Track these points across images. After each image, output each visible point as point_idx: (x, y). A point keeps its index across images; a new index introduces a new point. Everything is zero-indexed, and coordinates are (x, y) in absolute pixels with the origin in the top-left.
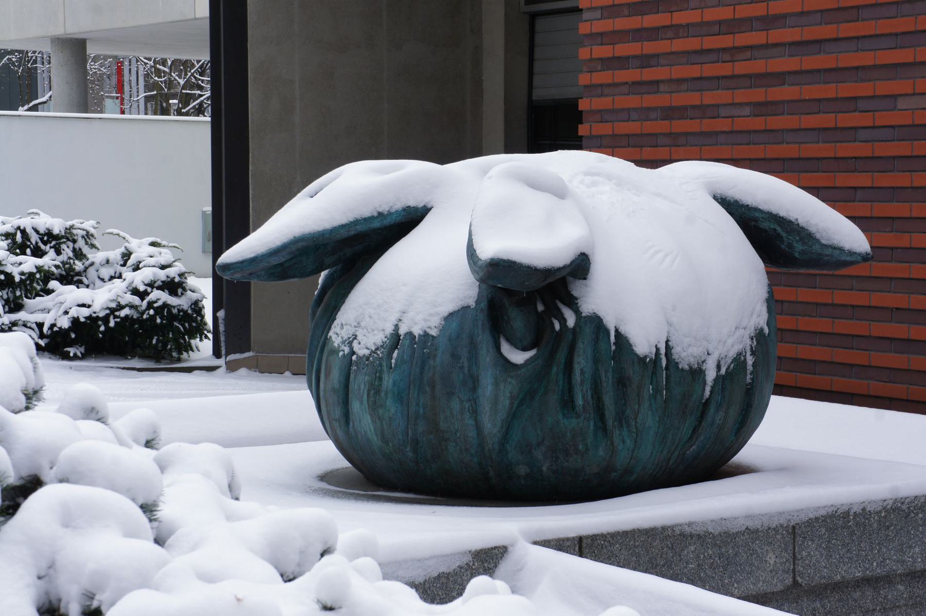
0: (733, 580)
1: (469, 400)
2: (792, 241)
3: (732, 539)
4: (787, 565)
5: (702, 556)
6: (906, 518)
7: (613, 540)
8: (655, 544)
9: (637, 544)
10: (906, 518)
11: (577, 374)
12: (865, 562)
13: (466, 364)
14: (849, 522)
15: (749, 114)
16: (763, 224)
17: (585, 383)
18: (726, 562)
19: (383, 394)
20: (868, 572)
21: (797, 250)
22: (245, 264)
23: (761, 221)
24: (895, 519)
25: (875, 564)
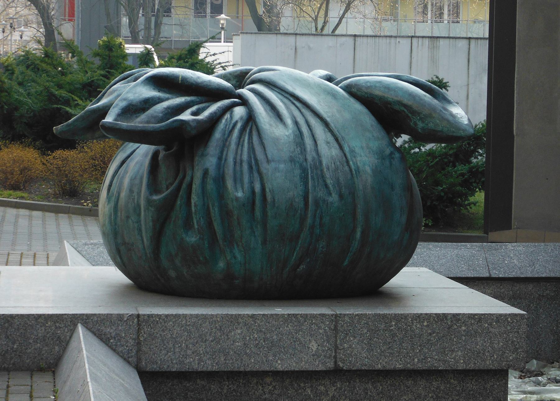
0: (277, 358)
1: (138, 222)
3: (277, 328)
5: (248, 338)
6: (449, 328)
7: (167, 318)
9: (188, 323)
13: (136, 197)
18: (270, 345)
24: (437, 328)
25: (416, 360)
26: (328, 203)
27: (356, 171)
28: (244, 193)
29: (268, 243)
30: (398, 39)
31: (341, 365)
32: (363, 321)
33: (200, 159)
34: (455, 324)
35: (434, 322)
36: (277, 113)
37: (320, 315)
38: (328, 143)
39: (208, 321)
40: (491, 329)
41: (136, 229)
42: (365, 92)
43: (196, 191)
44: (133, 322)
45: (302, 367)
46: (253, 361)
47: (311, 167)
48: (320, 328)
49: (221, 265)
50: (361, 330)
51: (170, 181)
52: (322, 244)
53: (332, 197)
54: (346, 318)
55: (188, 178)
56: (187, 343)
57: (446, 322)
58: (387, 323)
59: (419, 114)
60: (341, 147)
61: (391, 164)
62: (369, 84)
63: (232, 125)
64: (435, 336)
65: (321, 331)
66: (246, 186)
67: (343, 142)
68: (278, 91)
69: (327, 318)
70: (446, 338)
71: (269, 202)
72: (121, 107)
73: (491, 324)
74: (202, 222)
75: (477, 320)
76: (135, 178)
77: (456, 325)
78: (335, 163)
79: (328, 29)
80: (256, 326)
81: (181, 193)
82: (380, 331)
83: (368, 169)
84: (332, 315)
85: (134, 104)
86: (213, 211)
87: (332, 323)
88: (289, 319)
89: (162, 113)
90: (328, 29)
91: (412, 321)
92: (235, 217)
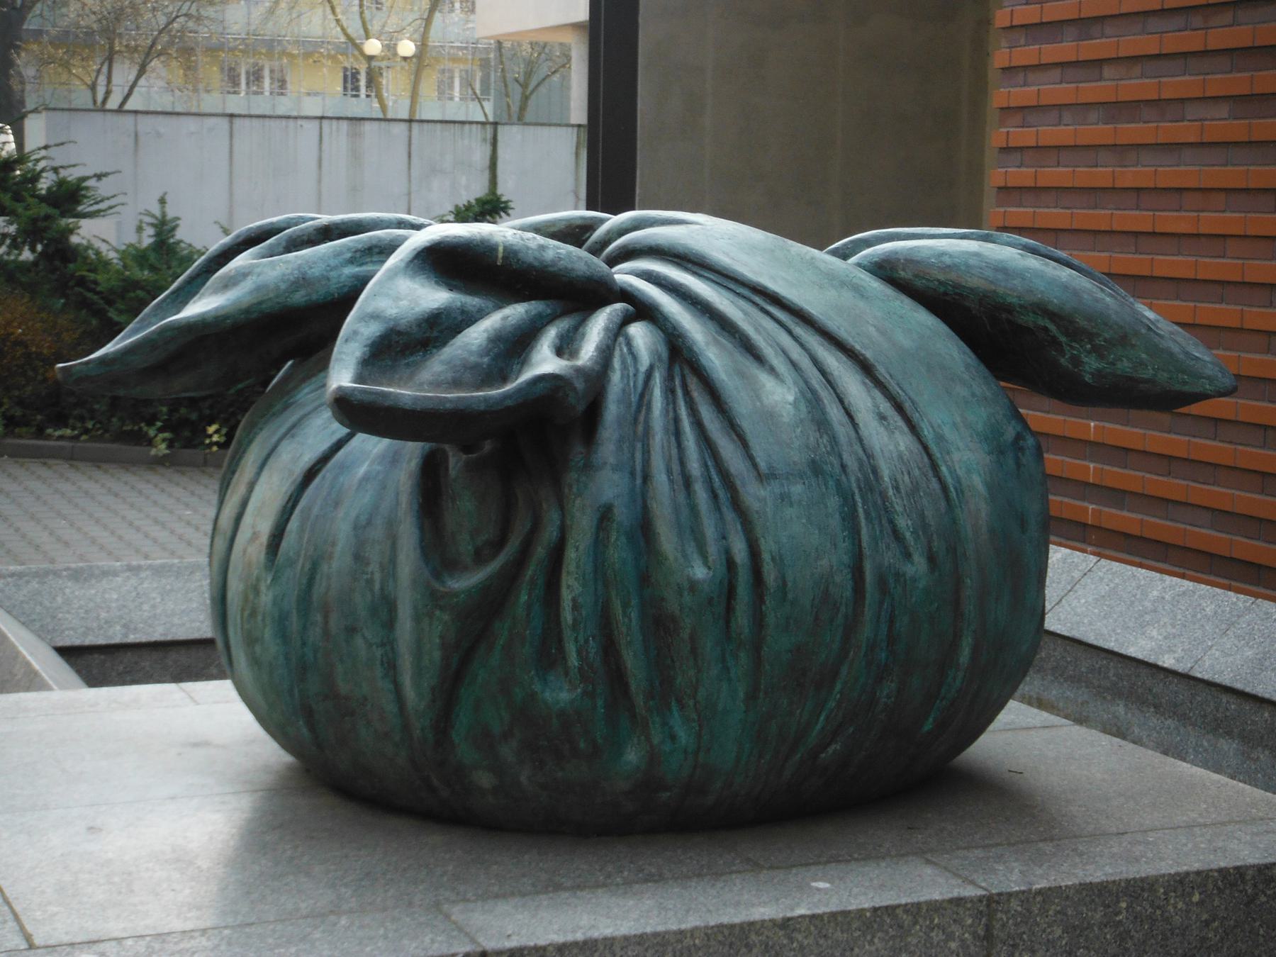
1: (383, 645)
2: (1079, 351)
3: (845, 950)
10: (1247, 904)
11: (567, 608)
13: (377, 576)
14: (1117, 914)
15: (1227, 116)
16: (1022, 317)
17: (582, 625)
19: (260, 618)
21: (1087, 368)
22: (91, 366)
23: (1018, 312)
24: (1223, 907)
26: (905, 581)
27: (956, 489)
28: (709, 568)
29: (761, 694)
30: (300, 122)
32: (1053, 907)
33: (584, 478)
34: (1264, 892)
35: (1215, 892)
36: (741, 340)
37: (951, 901)
38: (882, 418)
39: (670, 948)
41: (378, 662)
42: (938, 280)
43: (578, 567)
47: (860, 489)
48: (950, 937)
49: (632, 756)
50: (1049, 930)
51: (487, 536)
52: (888, 689)
53: (912, 564)
54: (1015, 905)
55: (550, 533)
57: (1241, 888)
58: (1109, 907)
59: (1091, 336)
60: (913, 428)
61: (1018, 464)
62: (947, 260)
63: (641, 378)
64: (1217, 928)
66: (713, 549)
67: (917, 414)
68: (718, 281)
69: (969, 909)
70: (1242, 931)
71: (772, 591)
72: (368, 339)
74: (593, 651)
76: (369, 523)
77: (1265, 895)
78: (909, 474)
79: (113, 103)
80: (794, 950)
81: (530, 573)
82: (1093, 930)
83: (977, 482)
84: (980, 899)
85: (402, 328)
86: (626, 620)
87: (980, 921)
88: (875, 921)
89: (488, 355)
90: (113, 103)
91: (1165, 893)
92: (685, 634)
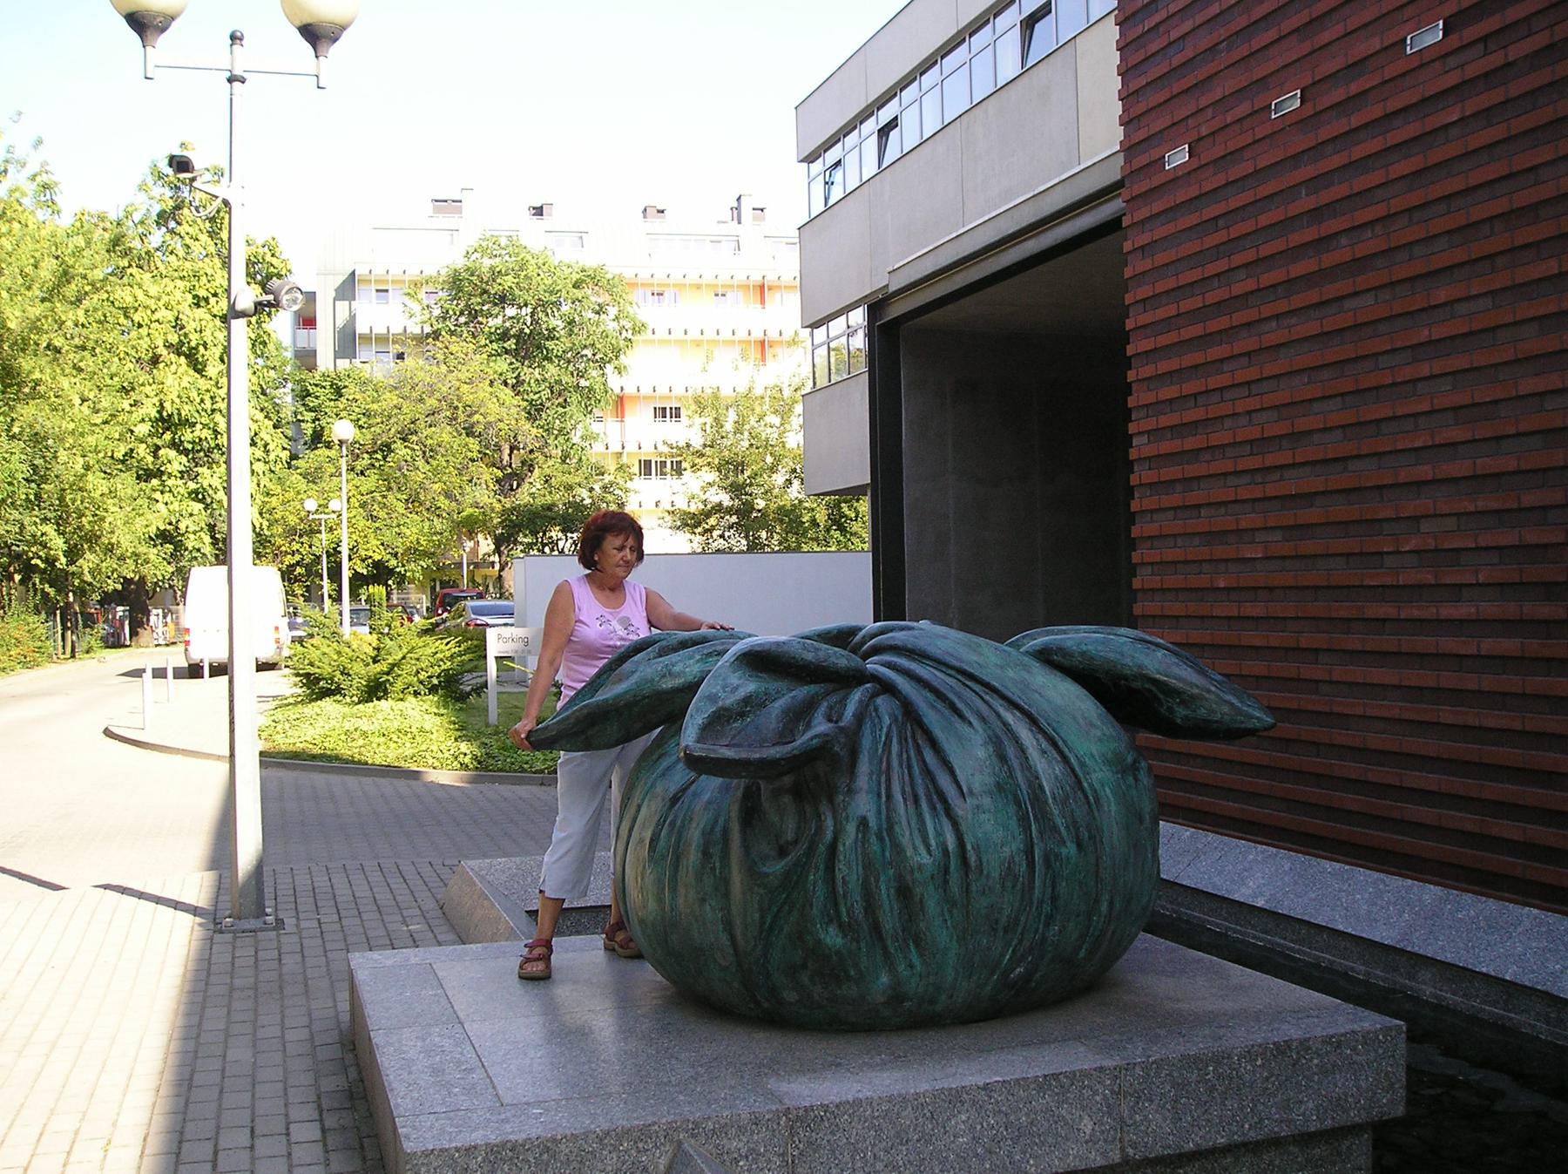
0: (1028, 1155)
1: (721, 909)
4: (1112, 1133)
5: (979, 1127)
6: (1294, 1065)
7: (839, 1110)
8: (904, 1114)
9: (876, 1114)
12: (1232, 1124)
18: (1016, 1133)
20: (1236, 1137)
22: (638, 726)
25: (1247, 1126)
31: (1131, 1152)
40: (1355, 1058)
44: (779, 1123)
45: (1069, 1165)
46: (988, 1166)
48: (1095, 1093)
56: (876, 1150)
65: (1098, 1098)
73: (1354, 1049)
75: (1335, 1045)
91: (1238, 1060)
